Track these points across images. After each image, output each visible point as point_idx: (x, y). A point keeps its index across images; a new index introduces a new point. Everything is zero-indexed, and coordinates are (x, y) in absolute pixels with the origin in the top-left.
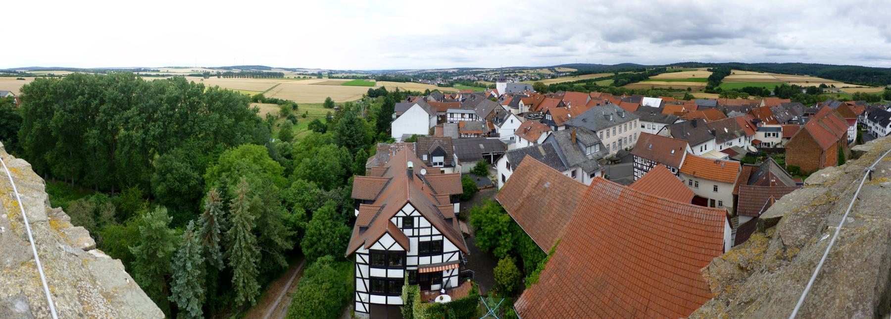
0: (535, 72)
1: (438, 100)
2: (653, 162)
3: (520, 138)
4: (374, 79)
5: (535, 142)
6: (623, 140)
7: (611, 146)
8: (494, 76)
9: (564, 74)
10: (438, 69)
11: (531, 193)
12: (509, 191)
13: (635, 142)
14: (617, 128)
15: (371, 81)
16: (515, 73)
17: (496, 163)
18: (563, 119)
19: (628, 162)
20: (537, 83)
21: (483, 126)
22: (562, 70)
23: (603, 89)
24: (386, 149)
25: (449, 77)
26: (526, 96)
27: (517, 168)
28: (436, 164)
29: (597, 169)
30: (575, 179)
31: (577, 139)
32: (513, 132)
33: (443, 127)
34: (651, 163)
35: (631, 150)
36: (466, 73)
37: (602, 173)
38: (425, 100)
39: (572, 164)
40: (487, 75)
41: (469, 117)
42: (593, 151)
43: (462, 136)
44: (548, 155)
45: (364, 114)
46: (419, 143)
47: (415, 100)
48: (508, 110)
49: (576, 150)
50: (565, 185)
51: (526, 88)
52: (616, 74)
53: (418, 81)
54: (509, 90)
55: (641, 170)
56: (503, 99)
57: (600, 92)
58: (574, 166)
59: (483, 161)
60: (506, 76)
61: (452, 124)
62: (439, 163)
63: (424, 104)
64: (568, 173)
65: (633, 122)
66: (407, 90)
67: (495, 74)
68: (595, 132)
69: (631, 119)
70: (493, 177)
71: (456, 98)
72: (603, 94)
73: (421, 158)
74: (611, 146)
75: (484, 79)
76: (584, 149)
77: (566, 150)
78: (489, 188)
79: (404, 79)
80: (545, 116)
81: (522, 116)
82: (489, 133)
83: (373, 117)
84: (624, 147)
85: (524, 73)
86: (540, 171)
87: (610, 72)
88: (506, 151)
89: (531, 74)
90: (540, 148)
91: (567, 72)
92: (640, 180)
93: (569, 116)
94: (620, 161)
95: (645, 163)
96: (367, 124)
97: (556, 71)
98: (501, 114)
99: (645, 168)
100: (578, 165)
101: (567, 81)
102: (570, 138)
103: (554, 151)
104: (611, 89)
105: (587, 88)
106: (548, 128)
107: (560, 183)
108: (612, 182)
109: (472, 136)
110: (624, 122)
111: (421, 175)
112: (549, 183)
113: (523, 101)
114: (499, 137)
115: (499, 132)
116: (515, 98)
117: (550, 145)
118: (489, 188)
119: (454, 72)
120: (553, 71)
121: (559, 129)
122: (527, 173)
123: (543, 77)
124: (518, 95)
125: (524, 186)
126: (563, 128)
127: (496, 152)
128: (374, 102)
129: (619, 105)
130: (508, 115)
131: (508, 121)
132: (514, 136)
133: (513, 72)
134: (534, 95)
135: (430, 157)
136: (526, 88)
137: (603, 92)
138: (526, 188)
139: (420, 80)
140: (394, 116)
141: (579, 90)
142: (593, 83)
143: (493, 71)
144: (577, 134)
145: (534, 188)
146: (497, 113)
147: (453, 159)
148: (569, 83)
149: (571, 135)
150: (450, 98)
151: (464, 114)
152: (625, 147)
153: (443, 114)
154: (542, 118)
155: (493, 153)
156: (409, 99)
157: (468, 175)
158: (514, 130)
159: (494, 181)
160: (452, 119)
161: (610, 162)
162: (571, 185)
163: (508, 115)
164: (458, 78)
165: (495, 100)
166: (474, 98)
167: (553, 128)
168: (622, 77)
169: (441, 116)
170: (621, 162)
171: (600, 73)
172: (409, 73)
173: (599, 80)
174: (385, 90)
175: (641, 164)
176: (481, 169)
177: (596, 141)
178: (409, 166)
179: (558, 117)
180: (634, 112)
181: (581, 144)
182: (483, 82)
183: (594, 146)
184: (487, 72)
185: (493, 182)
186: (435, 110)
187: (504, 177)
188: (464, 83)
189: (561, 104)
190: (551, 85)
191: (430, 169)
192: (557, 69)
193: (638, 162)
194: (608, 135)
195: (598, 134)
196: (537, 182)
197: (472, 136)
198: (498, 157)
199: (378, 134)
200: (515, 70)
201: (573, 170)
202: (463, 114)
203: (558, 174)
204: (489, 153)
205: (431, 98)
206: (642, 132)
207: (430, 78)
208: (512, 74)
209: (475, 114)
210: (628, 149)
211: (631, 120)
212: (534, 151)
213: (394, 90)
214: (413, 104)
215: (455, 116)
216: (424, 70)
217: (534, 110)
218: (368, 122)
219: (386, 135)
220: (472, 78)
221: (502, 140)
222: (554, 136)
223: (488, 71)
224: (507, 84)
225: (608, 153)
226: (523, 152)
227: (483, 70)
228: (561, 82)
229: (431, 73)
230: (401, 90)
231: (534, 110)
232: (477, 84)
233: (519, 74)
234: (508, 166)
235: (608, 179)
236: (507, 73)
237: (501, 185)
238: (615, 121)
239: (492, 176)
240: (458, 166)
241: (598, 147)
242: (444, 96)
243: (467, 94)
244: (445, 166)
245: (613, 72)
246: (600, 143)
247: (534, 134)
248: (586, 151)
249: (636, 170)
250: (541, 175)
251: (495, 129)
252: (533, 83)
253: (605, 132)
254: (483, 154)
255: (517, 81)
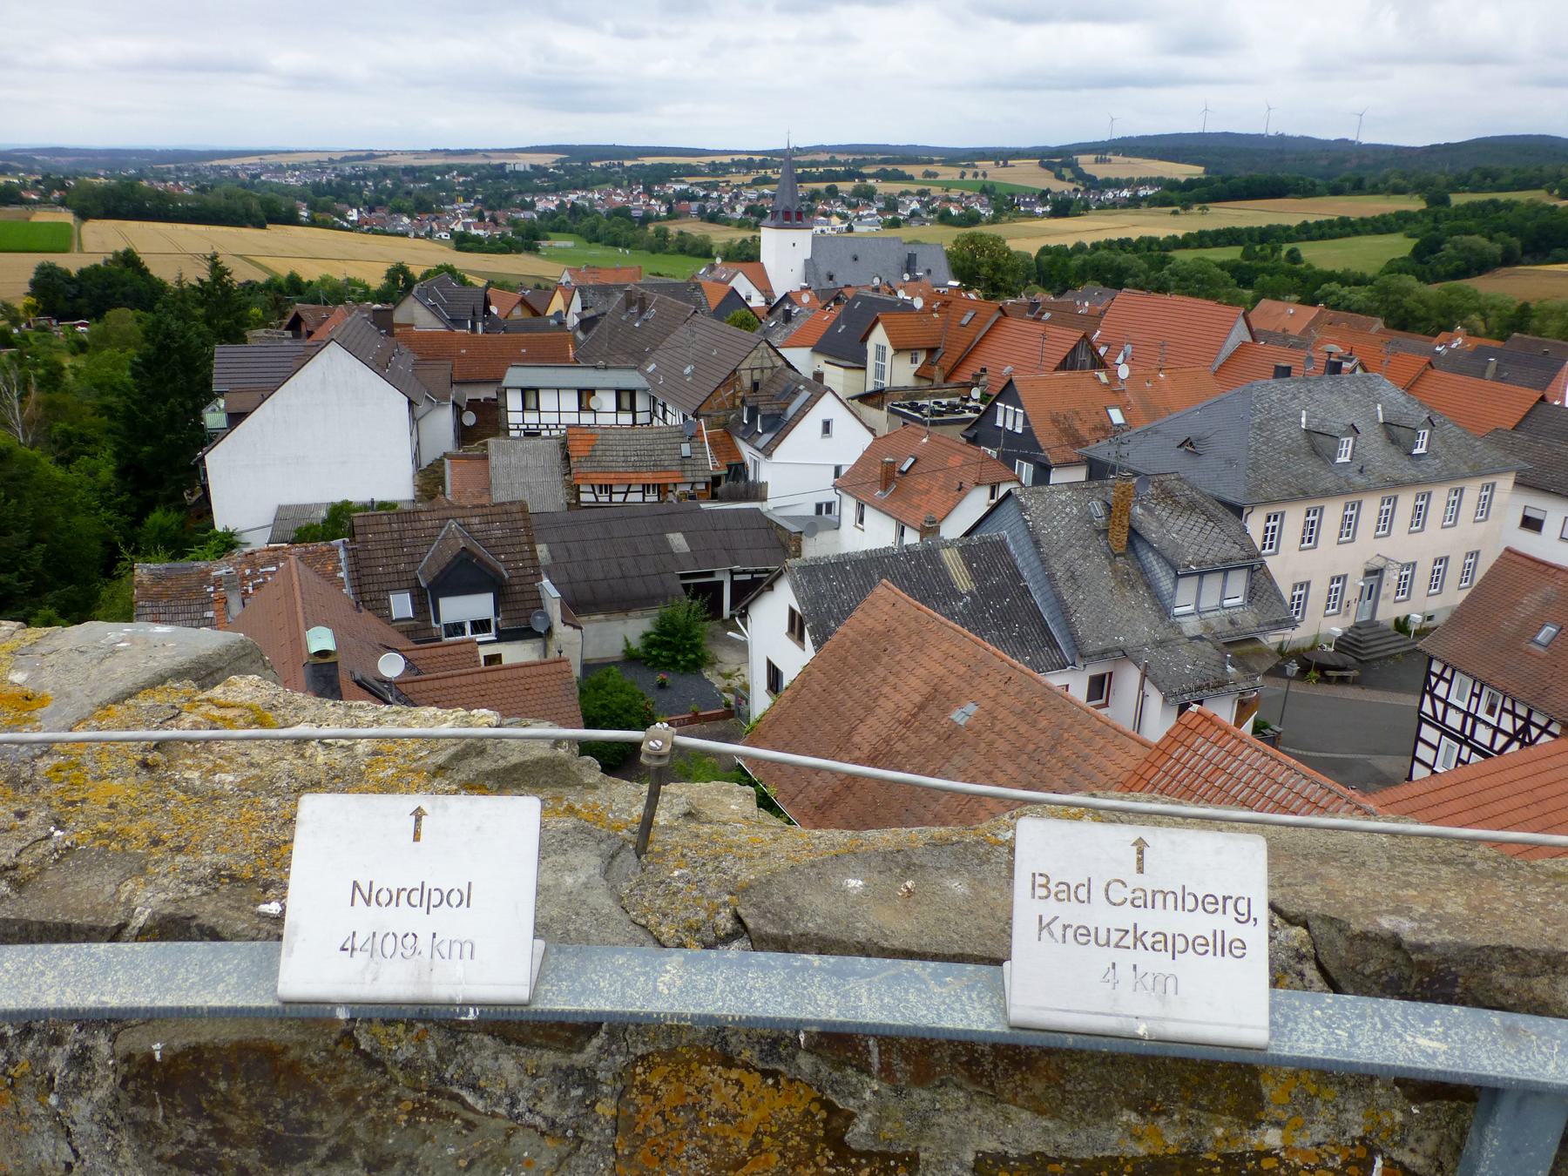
0: (969, 177)
1: (456, 322)
2: (1535, 718)
3: (861, 507)
4: (63, 203)
5: (929, 529)
6: (1392, 577)
7: (1318, 592)
8: (751, 194)
9: (1126, 193)
10: (448, 153)
11: (887, 741)
12: (795, 728)
13: (1455, 595)
14: (1371, 507)
15: (43, 216)
16: (863, 177)
17: (744, 616)
18: (1084, 432)
19: (1400, 688)
20: (972, 239)
21: (686, 449)
22: (1119, 168)
23: (1334, 286)
24: (188, 590)
25: (509, 195)
26: (907, 307)
27: (835, 638)
28: (457, 629)
29: (1218, 686)
30: (1102, 712)
31: (1134, 535)
32: (831, 479)
33: (485, 458)
34: (1528, 722)
35: (1422, 633)
36: (606, 178)
37: (1244, 708)
38: (383, 322)
39: (1093, 645)
40: (715, 186)
41: (619, 408)
42: (1210, 600)
43: (583, 497)
44: (984, 595)
45: (27, 424)
46: (365, 542)
47: (329, 325)
48: (807, 373)
49: (1124, 581)
50: (1043, 724)
51: (910, 264)
52: (1438, 200)
53: (342, 216)
54: (823, 269)
55: (1462, 742)
56: (788, 317)
57: (1314, 303)
58: (1103, 655)
59: (683, 608)
60: (814, 196)
61: (532, 442)
62: (474, 623)
63: (379, 343)
64: (1076, 684)
65: (1473, 491)
66: (283, 269)
67: (756, 182)
68: (1238, 511)
69: (1465, 469)
70: (729, 676)
71: (551, 312)
72: (1332, 313)
73: (380, 609)
74: (1318, 592)
75: (702, 211)
76: (1165, 583)
77: (1073, 577)
78: (708, 718)
79: (255, 206)
80: (992, 409)
81: (879, 406)
82: (716, 480)
83: (90, 432)
84: (1388, 612)
85: (910, 178)
86: (937, 655)
87: (1398, 191)
88: (790, 562)
89: (948, 186)
90: (950, 558)
91: (1143, 182)
92: (1434, 782)
93: (1117, 416)
94: (1352, 674)
95: (1491, 711)
96: (59, 473)
97: (1080, 176)
98: (776, 389)
99: (1483, 735)
100: (1124, 655)
101: (1134, 234)
102: (1100, 522)
103: (1017, 576)
104: (1385, 290)
105: (1243, 276)
106: (1002, 470)
107: (1022, 715)
108: (1293, 762)
109: (635, 497)
110: (1416, 483)
111: (384, 681)
112: (971, 708)
113: (886, 328)
114: (765, 499)
115: (762, 479)
116: (847, 317)
117: (1000, 547)
118: (708, 718)
119: (539, 171)
120: (1067, 173)
121: (1057, 477)
122: (876, 658)
123: (1006, 204)
124: (864, 299)
125: (860, 712)
126: (1080, 474)
127: (744, 569)
128: (80, 347)
129: (1409, 388)
130: (805, 395)
131: (809, 427)
132: (831, 496)
133: (849, 176)
134: (946, 304)
135: (425, 600)
136: (910, 264)
137: (1336, 307)
138: (871, 721)
139: (353, 215)
140: (213, 418)
141: (1198, 284)
142: (1286, 247)
143: (749, 165)
144: (1139, 510)
145: (906, 723)
146: (755, 386)
147: (538, 602)
148: (1150, 243)
149: (1108, 508)
150: (518, 313)
151: (592, 392)
152: (1399, 611)
153: (485, 393)
154: (978, 421)
155: (732, 573)
156: (296, 324)
157: (614, 669)
158: (838, 469)
159: (732, 691)
160: (531, 418)
161: (1293, 668)
162: (1071, 726)
163: (805, 395)
164: (561, 205)
165: (749, 321)
166: (642, 310)
167: (1026, 471)
168: (1471, 223)
169: (474, 405)
170: (1356, 682)
171: (1337, 191)
172: (279, 169)
173: (1322, 237)
174: (144, 272)
175: (1466, 714)
176: (676, 641)
177: (1235, 552)
178: (314, 648)
179: (1055, 421)
180: (1495, 437)
181: (1151, 560)
182: (694, 228)
183: (1220, 576)
184: (715, 168)
185: (730, 697)
186: (441, 373)
187: (774, 674)
188: (593, 229)
189: (1083, 357)
190: (1045, 250)
191: (424, 653)
192: (1087, 163)
193: (1452, 700)
194: (1310, 534)
195: (1255, 524)
196: (918, 699)
197: (631, 498)
198: (749, 591)
199: (138, 521)
200: (864, 163)
201: (1097, 669)
202: (585, 394)
203: (1015, 675)
204: (711, 574)
205: (416, 315)
206: (1508, 550)
207: (408, 203)
208: (845, 187)
209: (645, 390)
210: (1413, 628)
211: (1464, 477)
212: (919, 566)
213: (198, 273)
214: (319, 347)
215: (547, 401)
216: (371, 155)
217: (939, 377)
218: (64, 462)
219: (183, 524)
220: (639, 206)
221: (776, 517)
222: (1023, 508)
223: (719, 167)
224: (815, 239)
225: (1292, 624)
226: (870, 566)
227: (693, 161)
228: (1101, 237)
229: (410, 171)
230: (241, 274)
231: (939, 378)
232: (663, 234)
233: (883, 188)
234: (796, 626)
235: (1273, 741)
236: (820, 179)
237: (760, 702)
238: (1361, 471)
239: (726, 670)
240: (562, 632)
241: (1238, 584)
242: (487, 303)
243: (605, 291)
244: (504, 636)
245: (1420, 188)
246: (1254, 568)
247: (928, 492)
248: (1173, 596)
249: (1428, 733)
250: (941, 671)
251: (743, 464)
252: (946, 237)
253: (1294, 518)
254: (683, 577)
255: (868, 226)
